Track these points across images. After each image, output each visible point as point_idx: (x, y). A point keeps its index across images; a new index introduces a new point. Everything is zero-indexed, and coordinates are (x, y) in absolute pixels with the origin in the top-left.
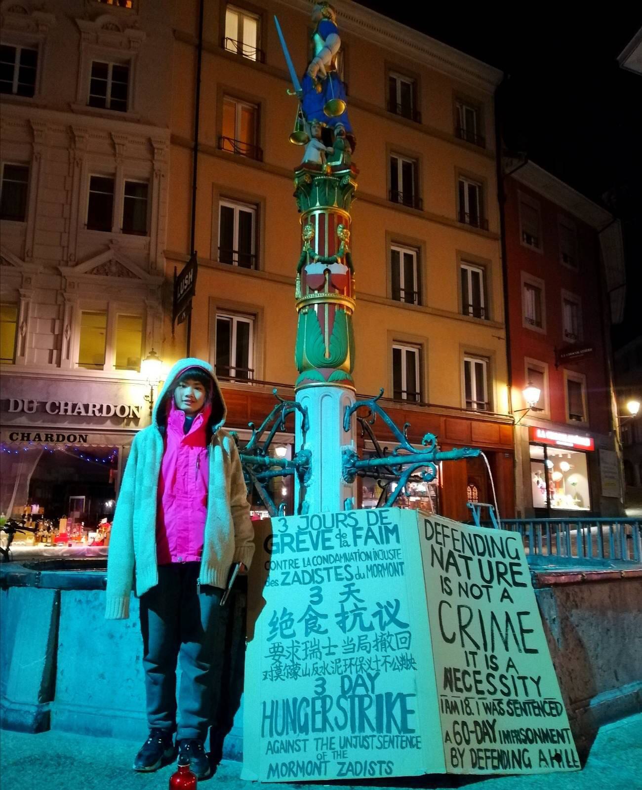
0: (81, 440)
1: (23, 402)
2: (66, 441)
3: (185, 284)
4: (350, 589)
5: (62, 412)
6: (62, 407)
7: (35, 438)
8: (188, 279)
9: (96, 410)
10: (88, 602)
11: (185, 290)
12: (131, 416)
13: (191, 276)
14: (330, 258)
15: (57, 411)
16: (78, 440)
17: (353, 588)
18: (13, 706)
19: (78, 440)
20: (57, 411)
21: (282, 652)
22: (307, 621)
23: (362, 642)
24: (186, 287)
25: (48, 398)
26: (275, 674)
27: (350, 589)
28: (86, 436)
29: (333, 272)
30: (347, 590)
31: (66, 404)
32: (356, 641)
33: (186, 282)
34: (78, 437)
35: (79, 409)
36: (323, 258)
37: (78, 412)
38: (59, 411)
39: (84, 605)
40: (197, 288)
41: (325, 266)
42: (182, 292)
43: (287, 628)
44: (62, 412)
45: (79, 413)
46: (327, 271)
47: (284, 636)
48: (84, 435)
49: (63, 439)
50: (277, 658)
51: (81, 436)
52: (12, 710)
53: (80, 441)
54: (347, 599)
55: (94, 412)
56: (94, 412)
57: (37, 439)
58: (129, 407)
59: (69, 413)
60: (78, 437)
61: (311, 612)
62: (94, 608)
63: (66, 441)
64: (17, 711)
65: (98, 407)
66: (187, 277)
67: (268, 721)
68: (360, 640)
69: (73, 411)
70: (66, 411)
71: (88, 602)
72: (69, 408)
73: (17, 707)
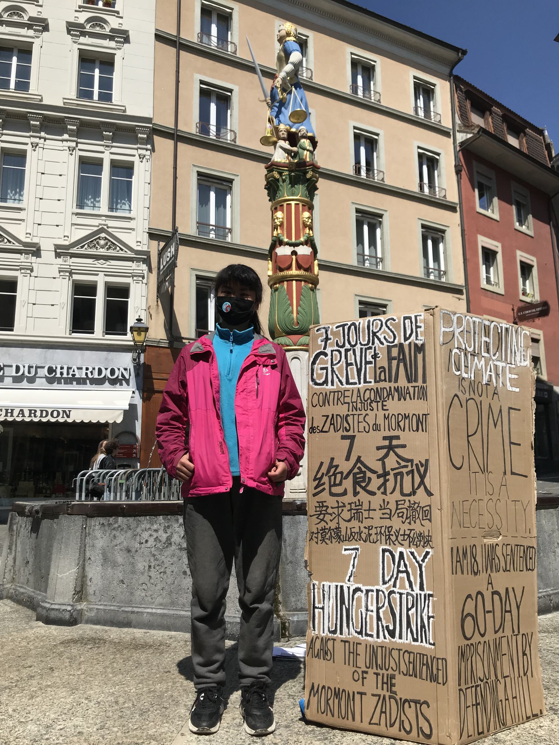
0: (65, 416)
1: (24, 367)
2: (49, 416)
3: (168, 257)
4: (390, 443)
5: (58, 375)
6: (59, 371)
7: (19, 414)
8: (170, 252)
9: (88, 372)
10: (110, 525)
11: (167, 262)
12: (120, 377)
13: (173, 249)
14: (298, 241)
15: (54, 373)
16: (61, 415)
17: (395, 442)
18: (53, 607)
19: (61, 415)
20: (54, 373)
21: (326, 510)
22: (355, 475)
23: (400, 507)
24: (168, 259)
25: (46, 363)
26: (320, 538)
27: (390, 443)
28: (70, 411)
29: (299, 253)
30: (387, 443)
31: (62, 368)
32: (393, 506)
33: (169, 255)
34: (61, 413)
35: (74, 371)
36: (290, 241)
37: (72, 375)
38: (56, 374)
39: (107, 528)
40: (179, 262)
41: (292, 249)
42: (164, 264)
43: (335, 485)
44: (58, 375)
45: (74, 375)
46: (294, 253)
47: (332, 494)
48: (67, 410)
49: (52, 412)
50: (321, 517)
51: (64, 412)
52: (53, 609)
53: (63, 417)
54: (387, 455)
55: (86, 374)
56: (86, 374)
57: (20, 415)
58: (119, 369)
59: (65, 375)
60: (61, 413)
61: (359, 465)
62: (114, 529)
63: (49, 416)
64: (57, 610)
65: (90, 369)
66: (169, 250)
67: (387, 421)
68: (397, 505)
69: (68, 374)
70: (62, 374)
71: (110, 525)
72: (65, 371)
73: (56, 607)
